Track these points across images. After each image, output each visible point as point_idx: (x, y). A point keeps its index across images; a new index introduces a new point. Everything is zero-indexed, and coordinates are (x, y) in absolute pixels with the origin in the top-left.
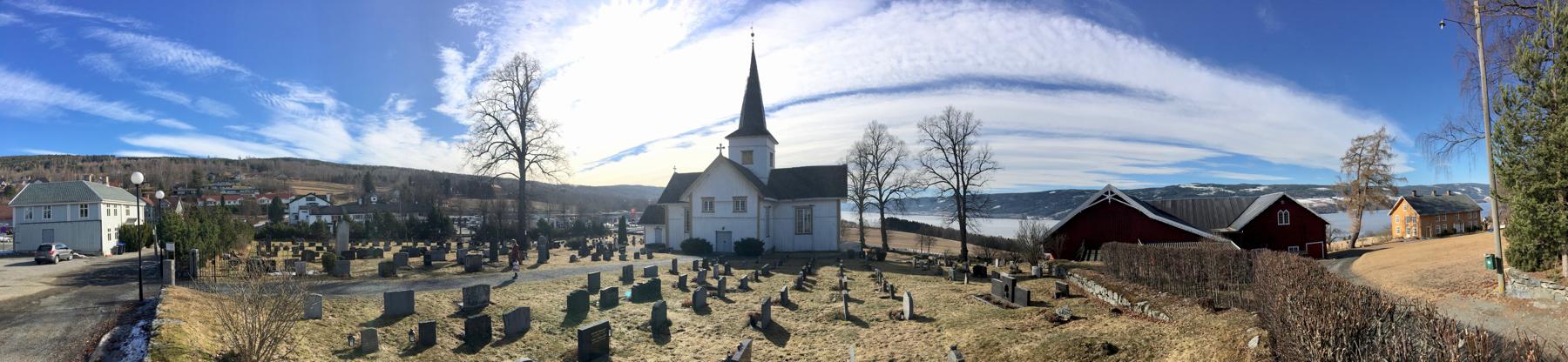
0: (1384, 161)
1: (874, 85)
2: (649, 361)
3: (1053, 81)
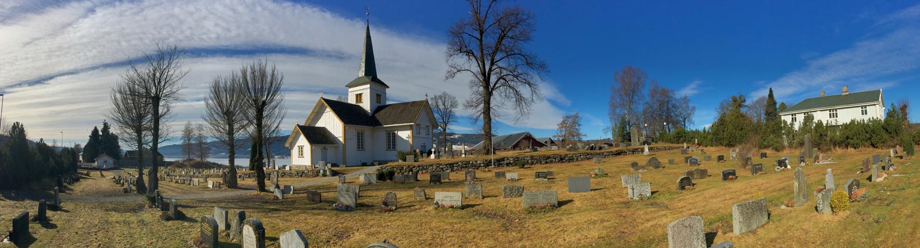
0: (577, 127)
1: (109, 61)
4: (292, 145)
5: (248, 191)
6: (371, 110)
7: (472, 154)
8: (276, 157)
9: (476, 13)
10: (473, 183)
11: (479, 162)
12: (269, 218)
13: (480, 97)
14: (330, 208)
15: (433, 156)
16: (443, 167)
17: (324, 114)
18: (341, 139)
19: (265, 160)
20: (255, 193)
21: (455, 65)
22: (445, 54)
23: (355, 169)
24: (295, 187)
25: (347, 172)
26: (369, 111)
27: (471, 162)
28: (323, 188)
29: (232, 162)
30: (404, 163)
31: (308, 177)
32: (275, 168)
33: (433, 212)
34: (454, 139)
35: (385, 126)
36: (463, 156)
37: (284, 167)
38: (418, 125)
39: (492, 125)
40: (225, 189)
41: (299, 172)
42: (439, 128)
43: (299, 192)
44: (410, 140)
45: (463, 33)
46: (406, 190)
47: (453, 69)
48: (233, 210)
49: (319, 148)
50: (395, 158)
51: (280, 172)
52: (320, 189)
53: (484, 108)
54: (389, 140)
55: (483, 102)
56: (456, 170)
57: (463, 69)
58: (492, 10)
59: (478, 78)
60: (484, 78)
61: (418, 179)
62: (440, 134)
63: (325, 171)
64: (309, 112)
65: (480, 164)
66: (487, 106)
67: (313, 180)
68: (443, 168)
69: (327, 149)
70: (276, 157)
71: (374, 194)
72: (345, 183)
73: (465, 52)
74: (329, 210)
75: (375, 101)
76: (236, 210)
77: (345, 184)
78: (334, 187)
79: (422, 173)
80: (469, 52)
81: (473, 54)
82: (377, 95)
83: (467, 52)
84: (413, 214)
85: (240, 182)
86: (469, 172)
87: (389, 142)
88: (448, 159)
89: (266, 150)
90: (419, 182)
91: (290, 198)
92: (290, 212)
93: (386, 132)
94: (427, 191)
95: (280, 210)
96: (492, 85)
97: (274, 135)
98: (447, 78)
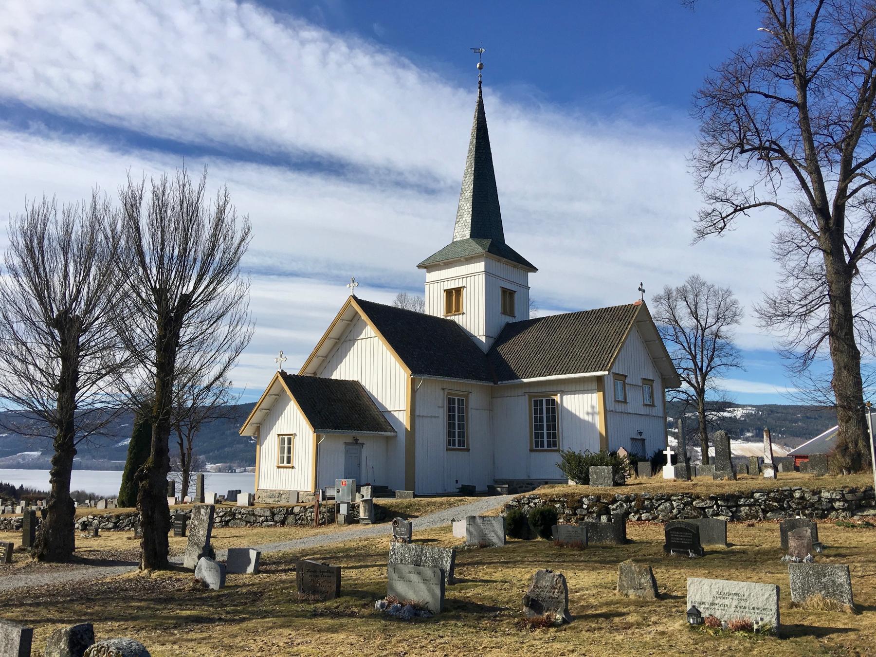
2: (862, 656)
3: (172, 133)
4: (261, 431)
5: (109, 569)
6: (487, 336)
7: (797, 469)
8: (209, 466)
9: (783, 26)
10: (812, 561)
11: (825, 495)
12: (174, 643)
13: (814, 284)
14: (366, 611)
15: (668, 471)
16: (702, 504)
17: (358, 344)
18: (403, 418)
19: (175, 477)
20: (132, 575)
21: (725, 192)
22: (694, 162)
23: (441, 504)
24: (264, 553)
25: (418, 510)
26: (483, 339)
27: (797, 495)
28: (348, 557)
29: (61, 478)
30: (582, 488)
31: (302, 525)
32: (203, 500)
33: (685, 638)
34: (733, 420)
35: (526, 380)
36: (769, 473)
37: (233, 495)
38: (620, 377)
39: (864, 373)
40: (29, 566)
41: (276, 511)
42: (684, 385)
43: (273, 567)
44: (599, 423)
45: (748, 92)
46: (594, 569)
47: (719, 206)
48: (50, 628)
49: (338, 443)
50: (557, 474)
51: (220, 510)
52: (338, 558)
53: (832, 320)
54: (538, 419)
55: (827, 299)
56: (747, 518)
57: (753, 203)
58: (831, 9)
59: (804, 226)
60: (822, 222)
61: (628, 537)
62: (687, 404)
63: (353, 508)
64: (315, 337)
65: (832, 501)
66: (840, 309)
67: (317, 534)
68: (703, 509)
69: (363, 444)
70: (209, 466)
71: (498, 576)
72: (411, 542)
73: (754, 149)
74: (362, 617)
75: (499, 307)
76: (60, 626)
77: (413, 546)
78: (379, 555)
79: (639, 519)
80: (770, 149)
81: (781, 151)
82: (505, 291)
83: (760, 148)
84: (619, 637)
85: (82, 542)
86: (793, 525)
87: (538, 427)
88: (719, 481)
89: (181, 445)
90: (631, 548)
91: (245, 585)
92: (244, 625)
93: (530, 398)
94: (660, 574)
95: (210, 620)
96: (851, 243)
97: (208, 402)
98: (702, 234)
